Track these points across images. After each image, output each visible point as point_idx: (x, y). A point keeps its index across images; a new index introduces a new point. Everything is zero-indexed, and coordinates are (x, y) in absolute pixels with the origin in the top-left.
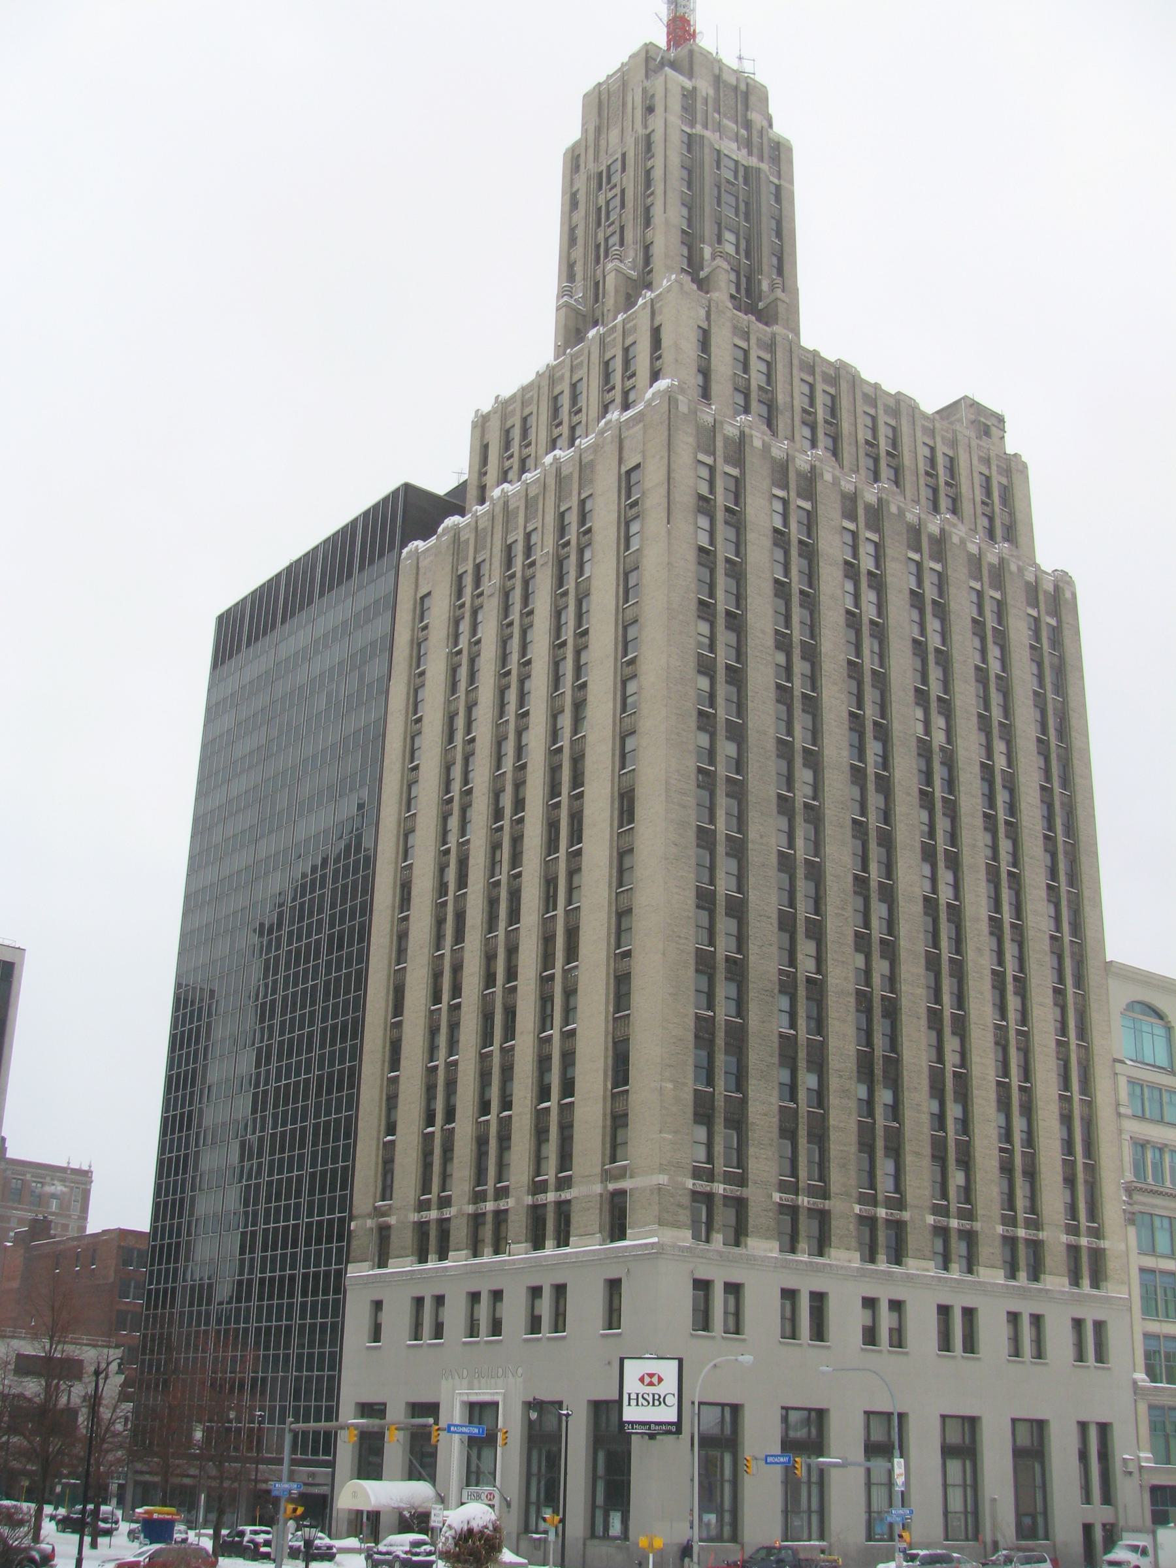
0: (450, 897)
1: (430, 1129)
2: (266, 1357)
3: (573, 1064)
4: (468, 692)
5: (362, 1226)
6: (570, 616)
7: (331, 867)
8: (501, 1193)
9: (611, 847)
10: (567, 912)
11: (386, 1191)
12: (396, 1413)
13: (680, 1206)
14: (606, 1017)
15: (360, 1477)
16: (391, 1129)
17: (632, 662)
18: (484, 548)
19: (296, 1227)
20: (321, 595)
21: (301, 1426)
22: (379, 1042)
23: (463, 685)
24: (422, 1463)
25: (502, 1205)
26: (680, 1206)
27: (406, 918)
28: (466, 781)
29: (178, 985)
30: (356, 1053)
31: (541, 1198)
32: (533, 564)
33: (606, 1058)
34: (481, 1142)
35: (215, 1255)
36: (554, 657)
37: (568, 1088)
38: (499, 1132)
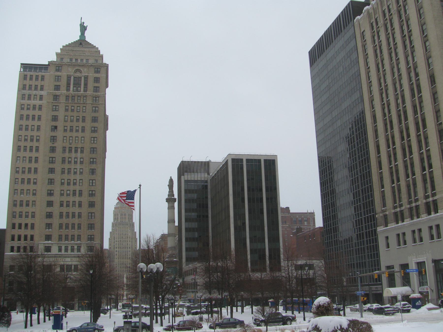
0: (387, 117)
1: (393, 185)
2: (359, 257)
3: (431, 159)
4: (381, 57)
5: (379, 216)
6: (405, 27)
8: (416, 200)
9: (430, 93)
10: (421, 115)
11: (384, 205)
12: (397, 268)
14: (438, 144)
15: (390, 287)
16: (383, 187)
17: (426, 36)
18: (377, 13)
19: (361, 219)
20: (335, 39)
21: (362, 275)
23: (379, 55)
24: (406, 281)
25: (417, 204)
27: (376, 126)
28: (385, 82)
29: (319, 157)
30: (369, 167)
31: (428, 200)
32: (391, 14)
33: (440, 155)
34: (408, 186)
35: (347, 229)
36: (403, 40)
37: (430, 166)
38: (413, 183)
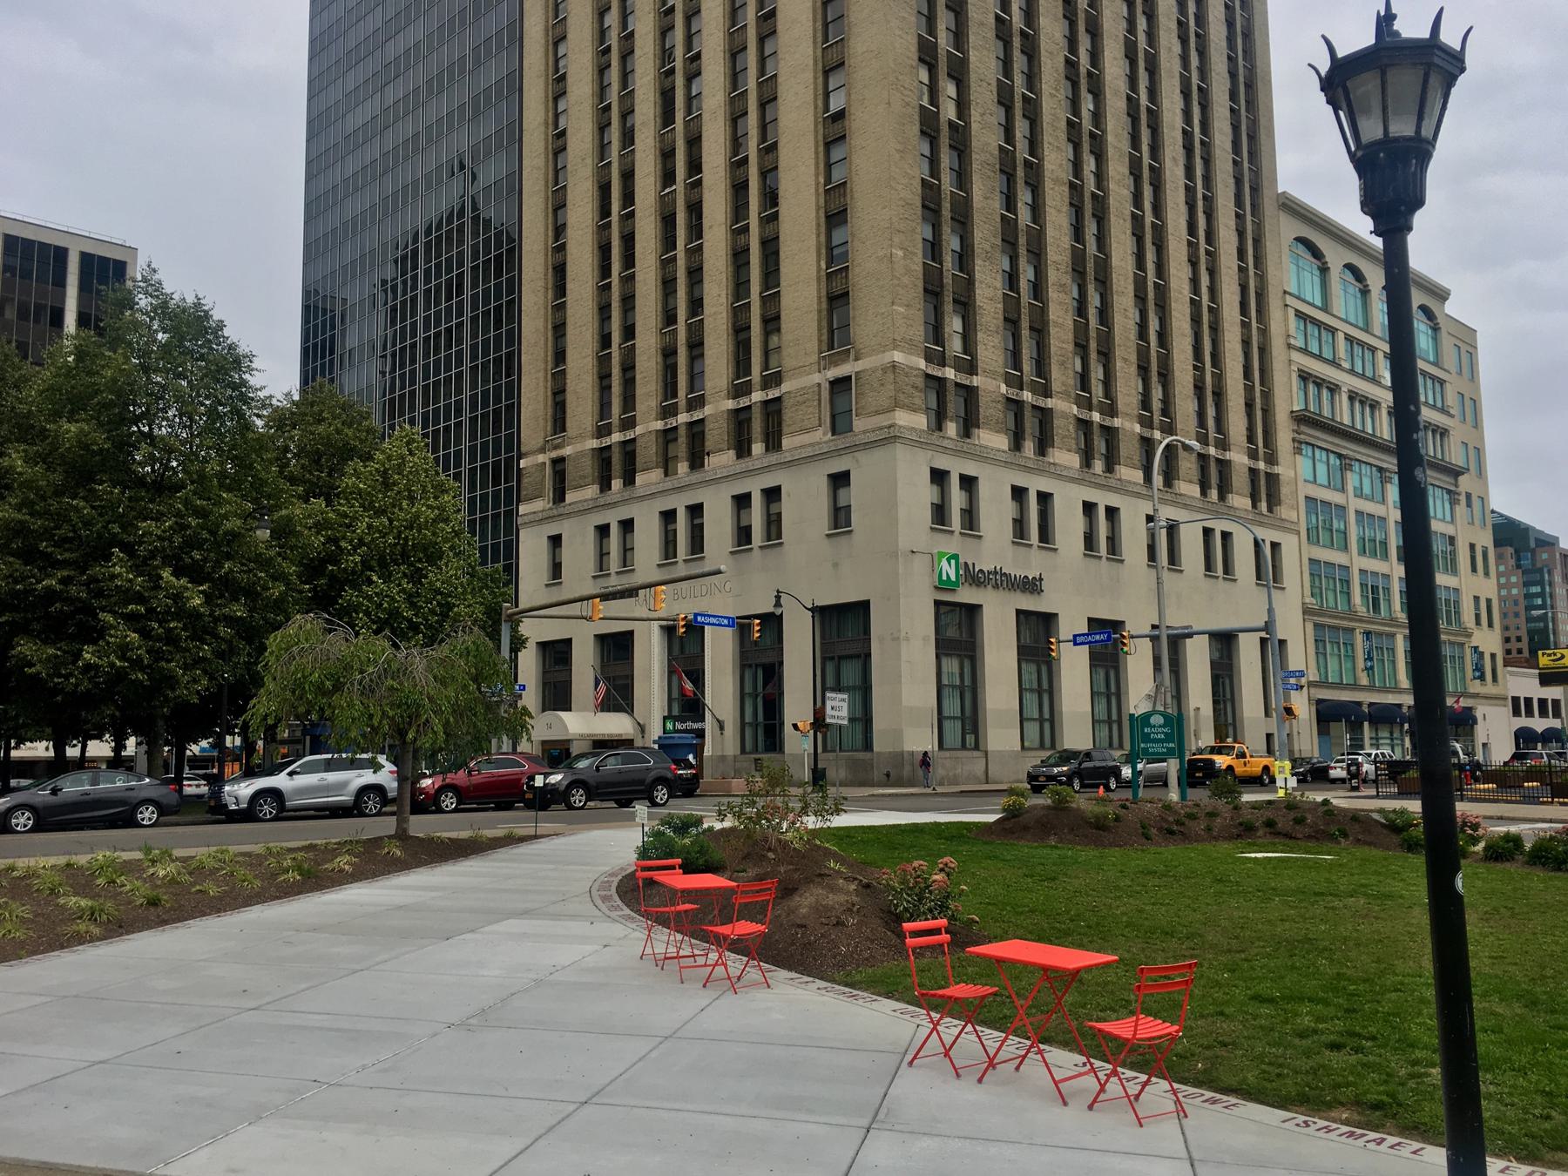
5: (533, 462)
7: (422, 239)
11: (559, 421)
13: (915, 387)
22: (541, 269)
26: (915, 387)
33: (818, 235)
